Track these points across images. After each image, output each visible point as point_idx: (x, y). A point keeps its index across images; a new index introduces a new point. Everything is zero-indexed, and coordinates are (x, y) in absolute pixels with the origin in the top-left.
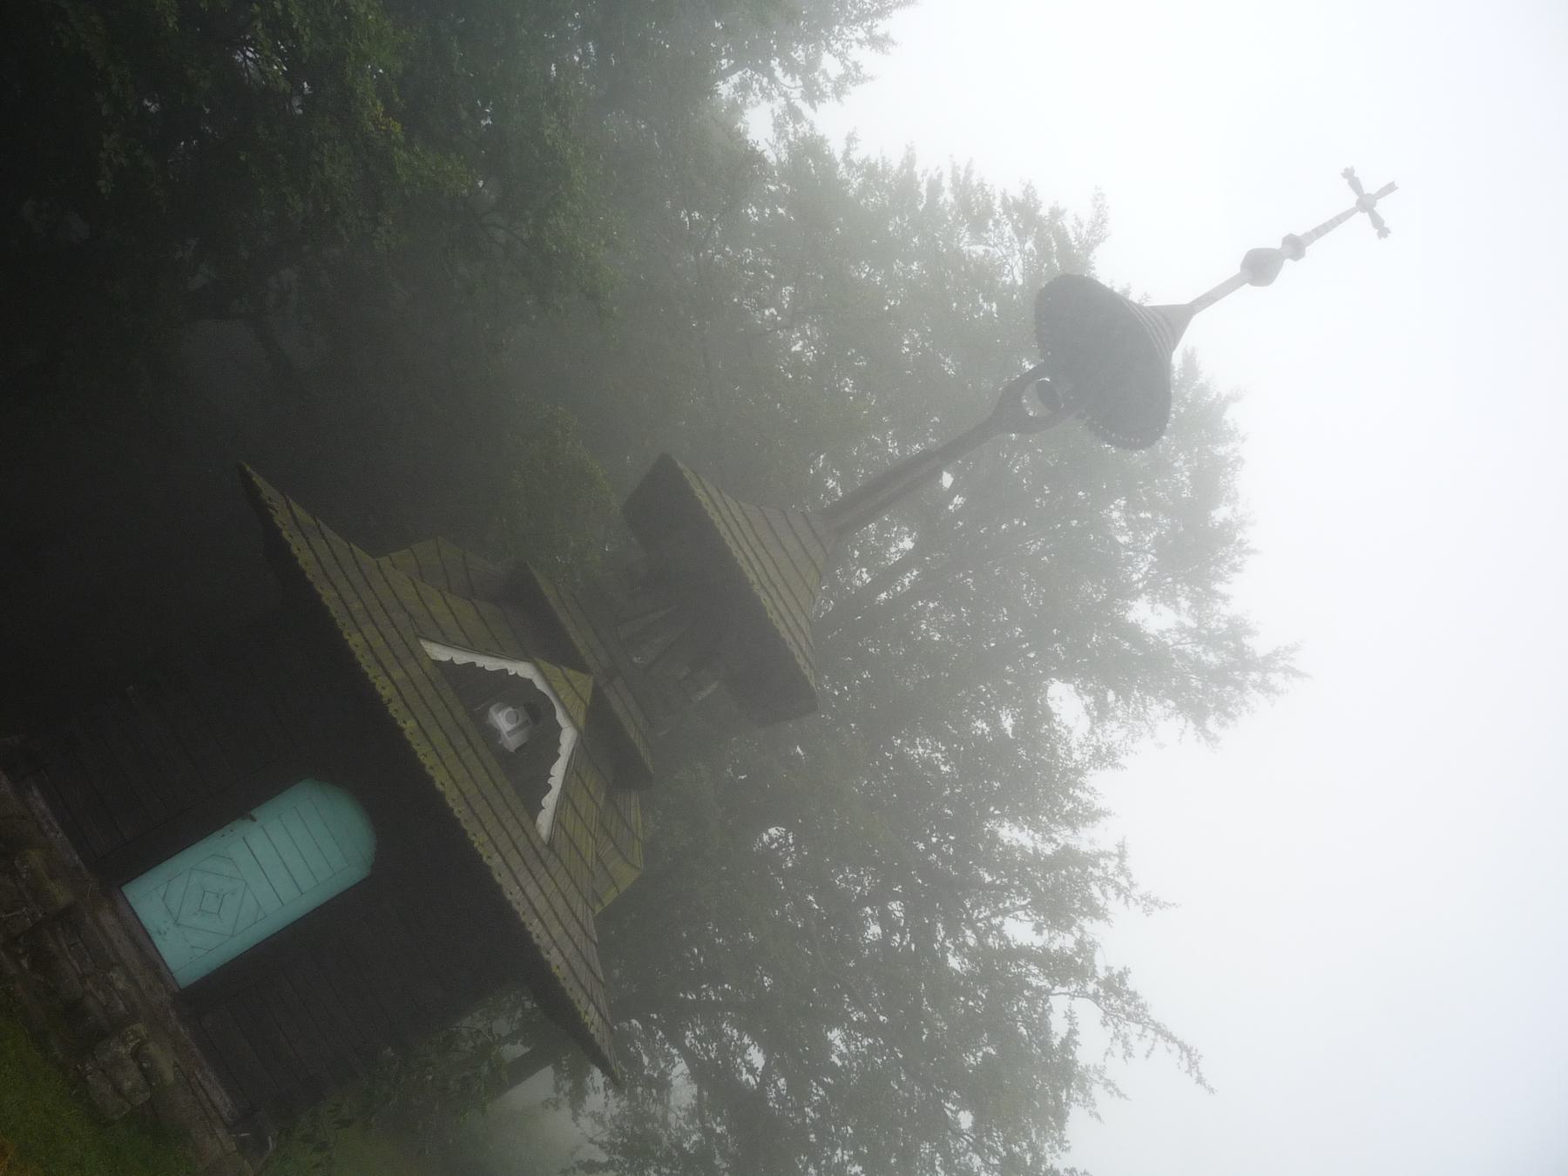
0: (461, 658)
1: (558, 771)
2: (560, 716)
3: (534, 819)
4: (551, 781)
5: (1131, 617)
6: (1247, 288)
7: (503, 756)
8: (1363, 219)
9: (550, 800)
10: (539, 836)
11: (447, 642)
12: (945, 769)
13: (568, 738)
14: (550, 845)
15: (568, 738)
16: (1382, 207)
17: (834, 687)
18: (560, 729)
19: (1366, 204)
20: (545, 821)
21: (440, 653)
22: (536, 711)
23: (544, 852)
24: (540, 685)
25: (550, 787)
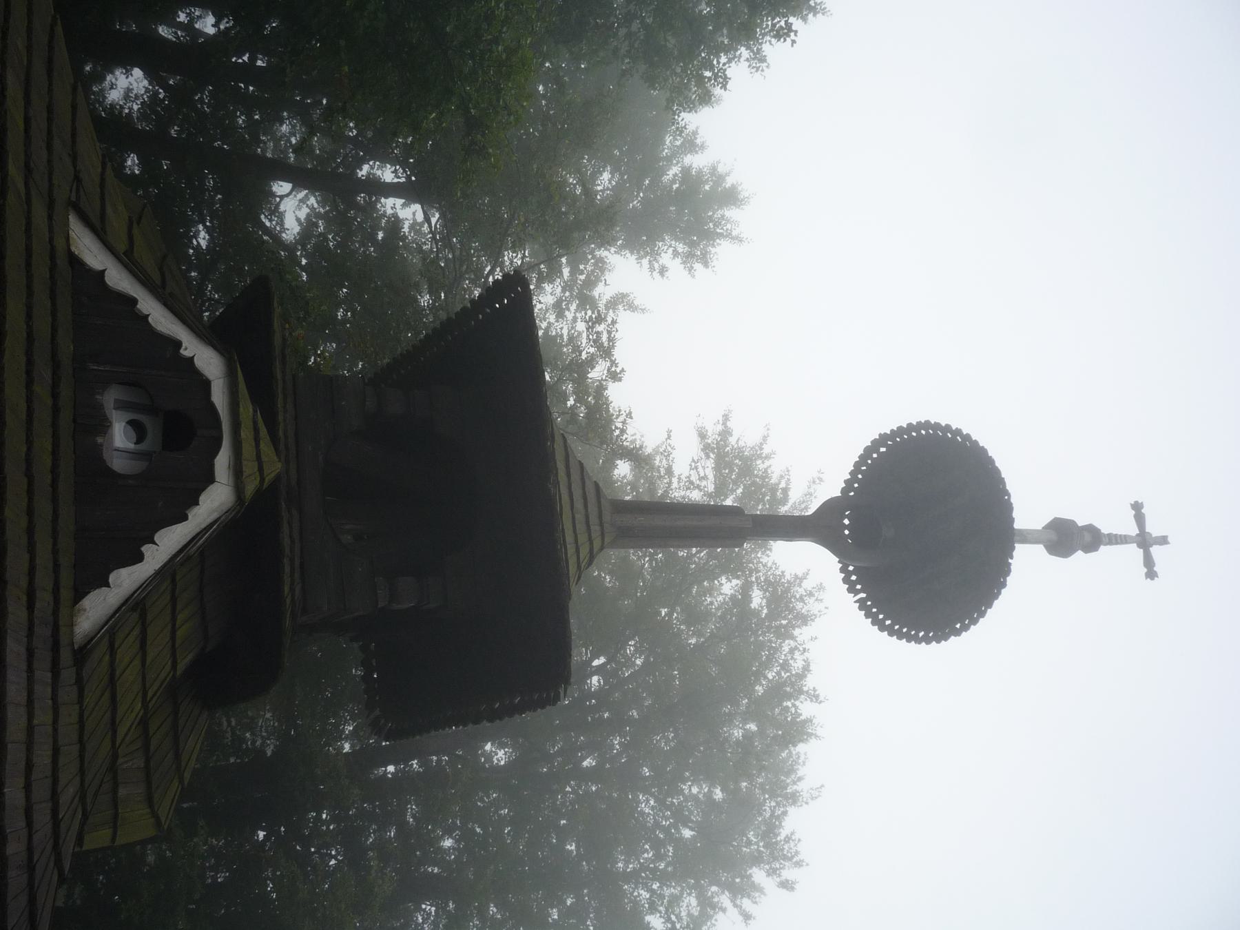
0: (119, 279)
1: (169, 541)
2: (222, 461)
3: (80, 594)
4: (147, 549)
5: (143, 549)
6: (1105, 531)
7: (92, 466)
8: (1133, 553)
9: (126, 580)
10: (72, 625)
11: (99, 231)
12: (380, 235)
13: (215, 501)
14: (82, 654)
15: (215, 501)
16: (1155, 550)
17: (588, 895)
18: (210, 479)
19: (1144, 541)
20: (96, 608)
21: (93, 254)
22: (182, 432)
23: (66, 656)
24: (219, 397)
25: (139, 558)
